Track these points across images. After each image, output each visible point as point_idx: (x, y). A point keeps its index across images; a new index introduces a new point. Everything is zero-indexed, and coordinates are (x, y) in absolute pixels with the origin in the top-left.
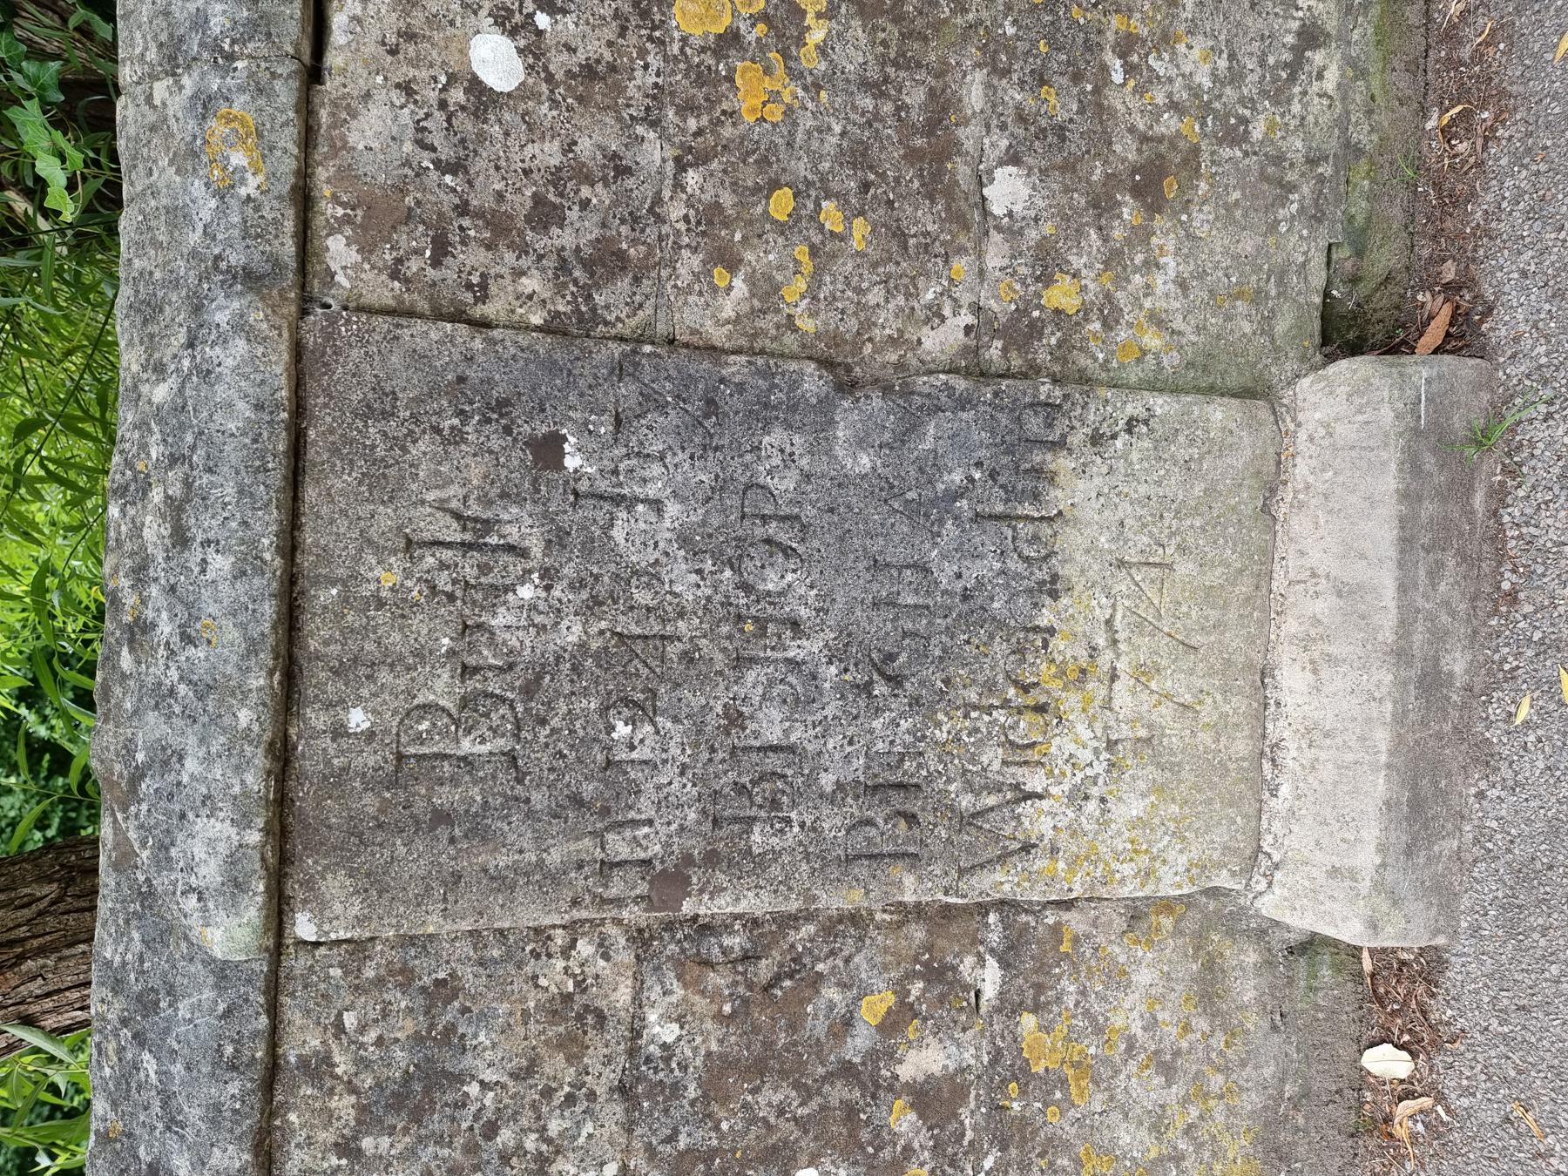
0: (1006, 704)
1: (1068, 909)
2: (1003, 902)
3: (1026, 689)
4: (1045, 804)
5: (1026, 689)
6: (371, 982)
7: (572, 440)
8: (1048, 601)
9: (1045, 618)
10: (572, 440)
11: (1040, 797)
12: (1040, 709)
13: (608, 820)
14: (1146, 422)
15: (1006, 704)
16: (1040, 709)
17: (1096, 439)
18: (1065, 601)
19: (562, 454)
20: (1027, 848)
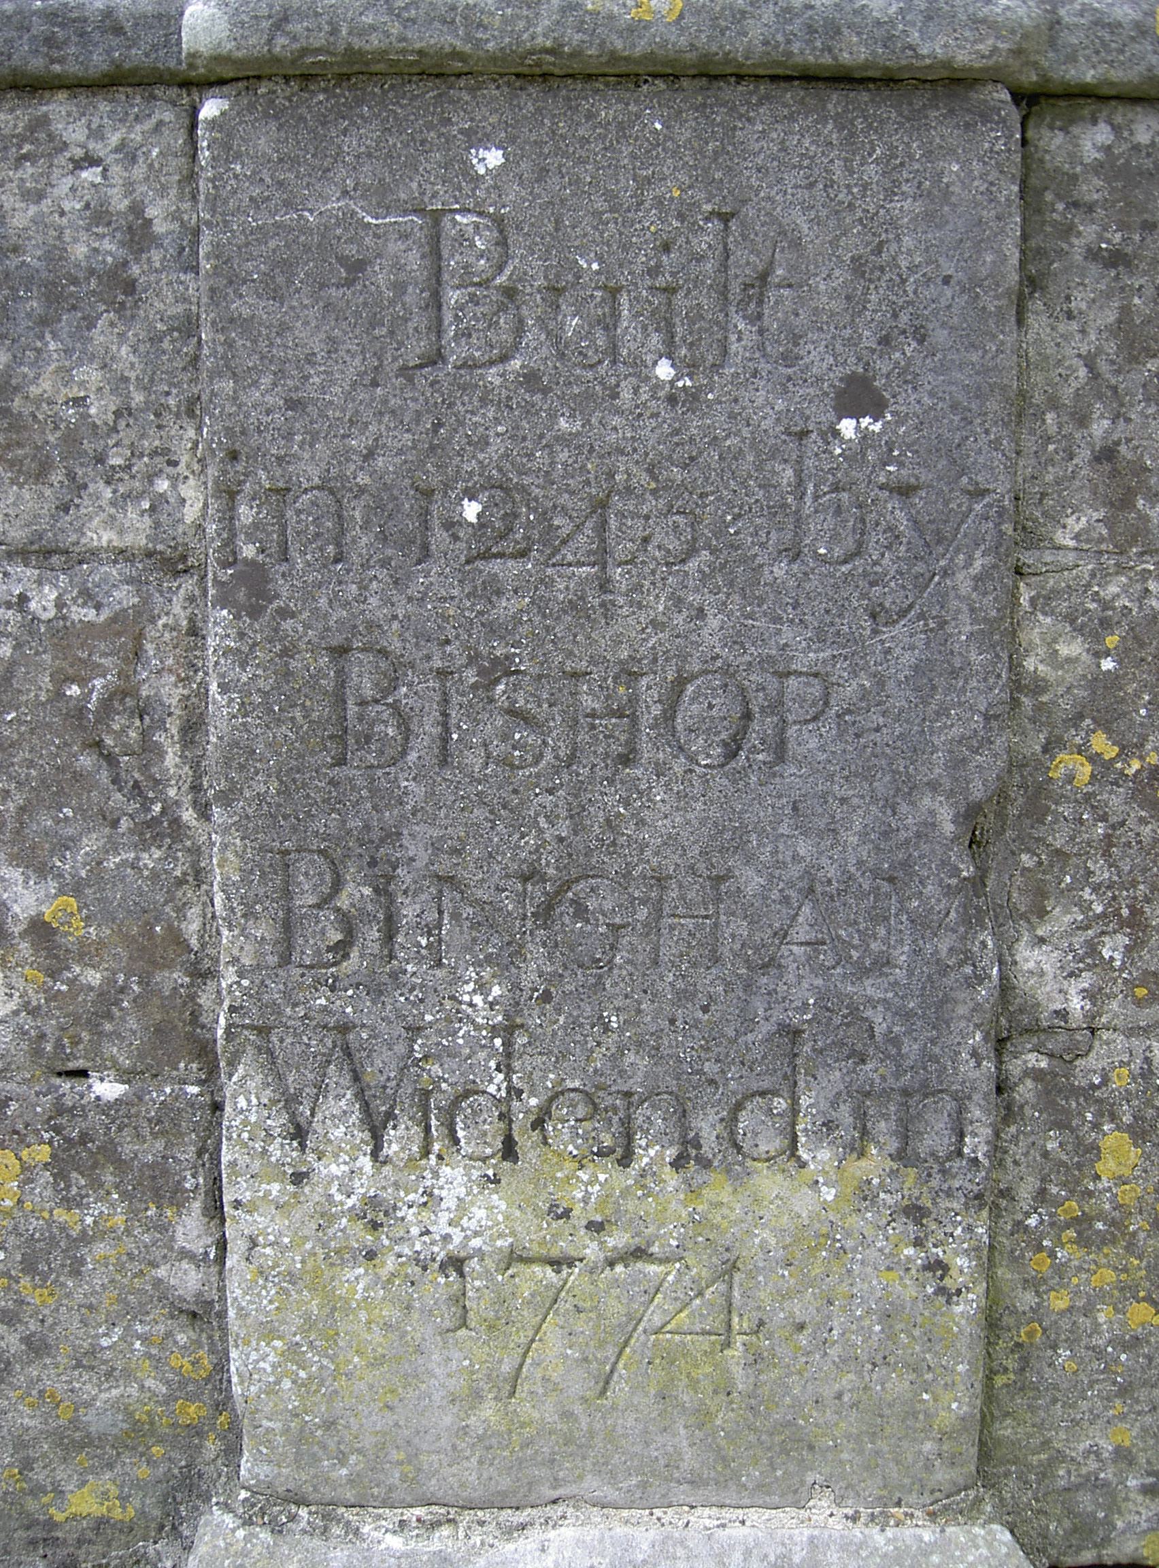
0: (515, 1092)
1: (206, 1211)
2: (217, 1107)
3: (538, 1124)
4: (366, 1162)
5: (538, 1124)
6: (932, 1553)
7: (877, 427)
8: (671, 1153)
9: (647, 1154)
10: (877, 427)
11: (375, 1155)
12: (509, 1151)
13: (884, 707)
14: (941, 1291)
15: (515, 1092)
16: (509, 1151)
17: (915, 1212)
18: (672, 1180)
19: (857, 416)
20: (299, 1133)
